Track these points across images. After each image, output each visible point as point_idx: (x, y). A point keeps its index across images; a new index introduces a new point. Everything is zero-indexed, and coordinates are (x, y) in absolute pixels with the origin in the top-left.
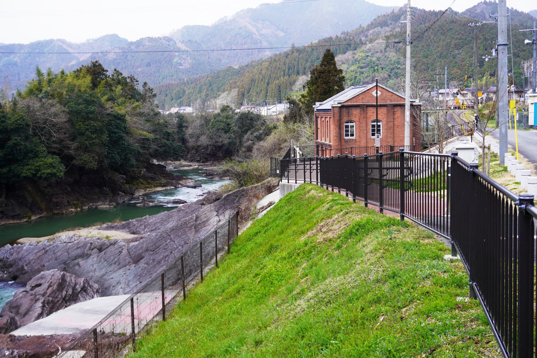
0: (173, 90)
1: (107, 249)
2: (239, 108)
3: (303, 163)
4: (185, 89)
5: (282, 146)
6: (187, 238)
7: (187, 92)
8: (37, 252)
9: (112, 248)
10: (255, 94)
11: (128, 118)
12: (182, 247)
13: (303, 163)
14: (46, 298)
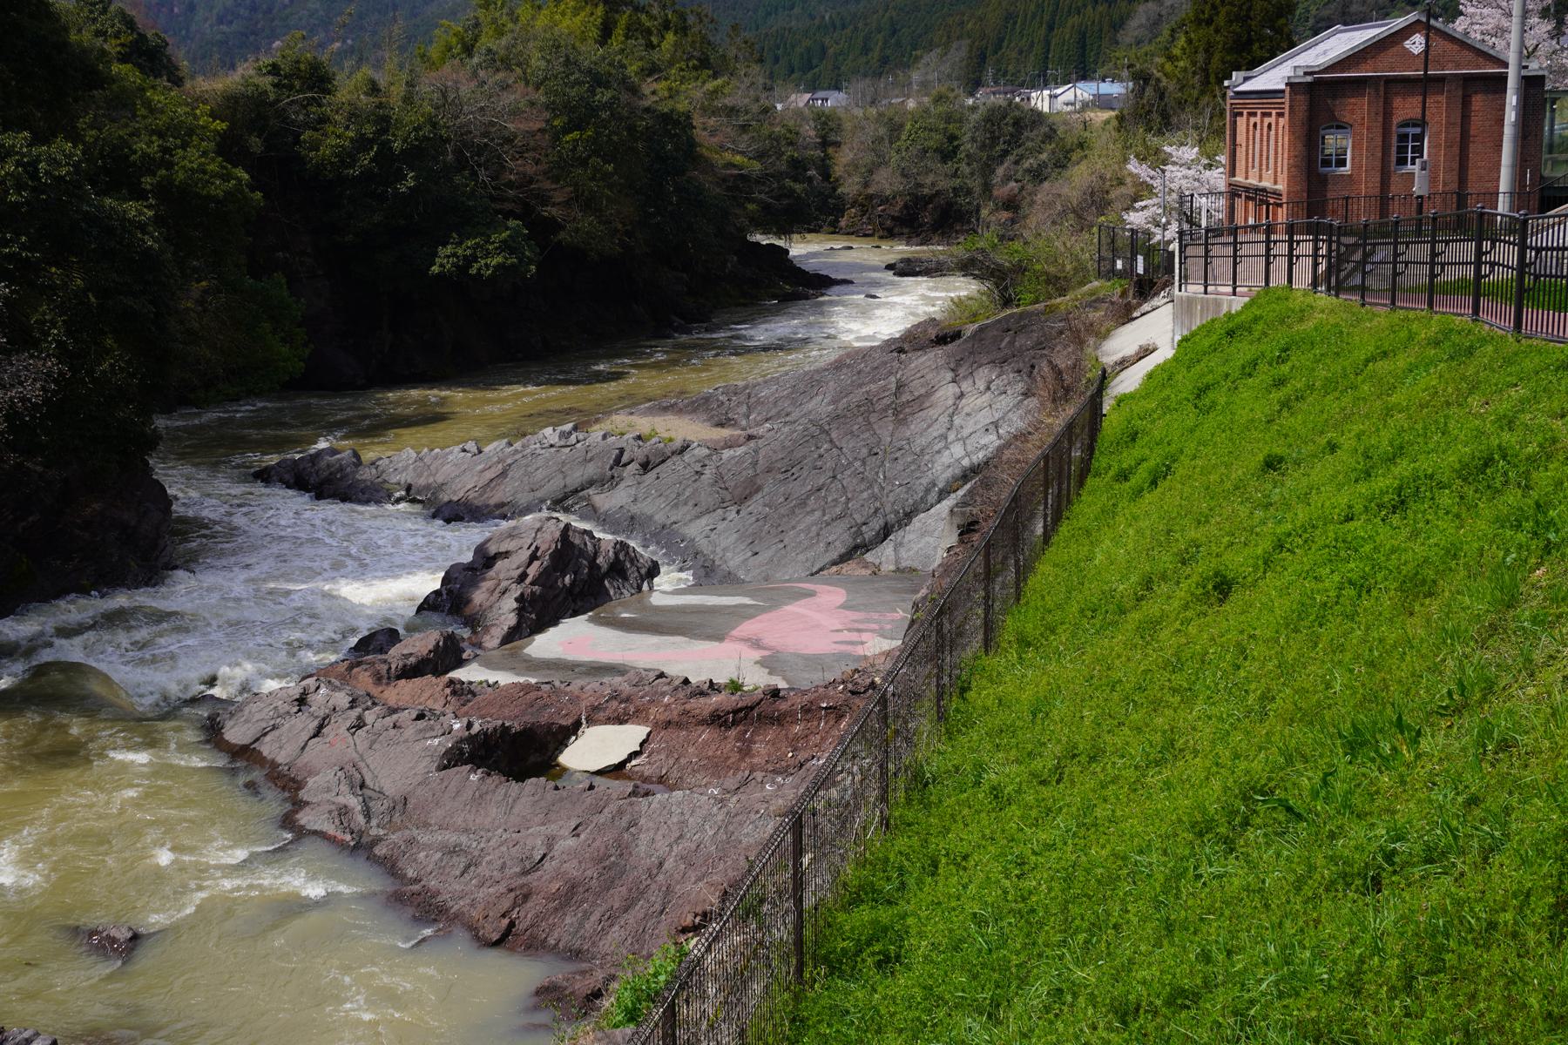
0: (793, 47)
1: (663, 466)
2: (972, 94)
3: (1231, 239)
4: (827, 41)
5: (1112, 195)
6: (873, 440)
7: (831, 51)
8: (484, 470)
9: (676, 464)
10: (1014, 55)
11: (697, 121)
12: (864, 462)
13: (1231, 239)
14: (526, 588)
